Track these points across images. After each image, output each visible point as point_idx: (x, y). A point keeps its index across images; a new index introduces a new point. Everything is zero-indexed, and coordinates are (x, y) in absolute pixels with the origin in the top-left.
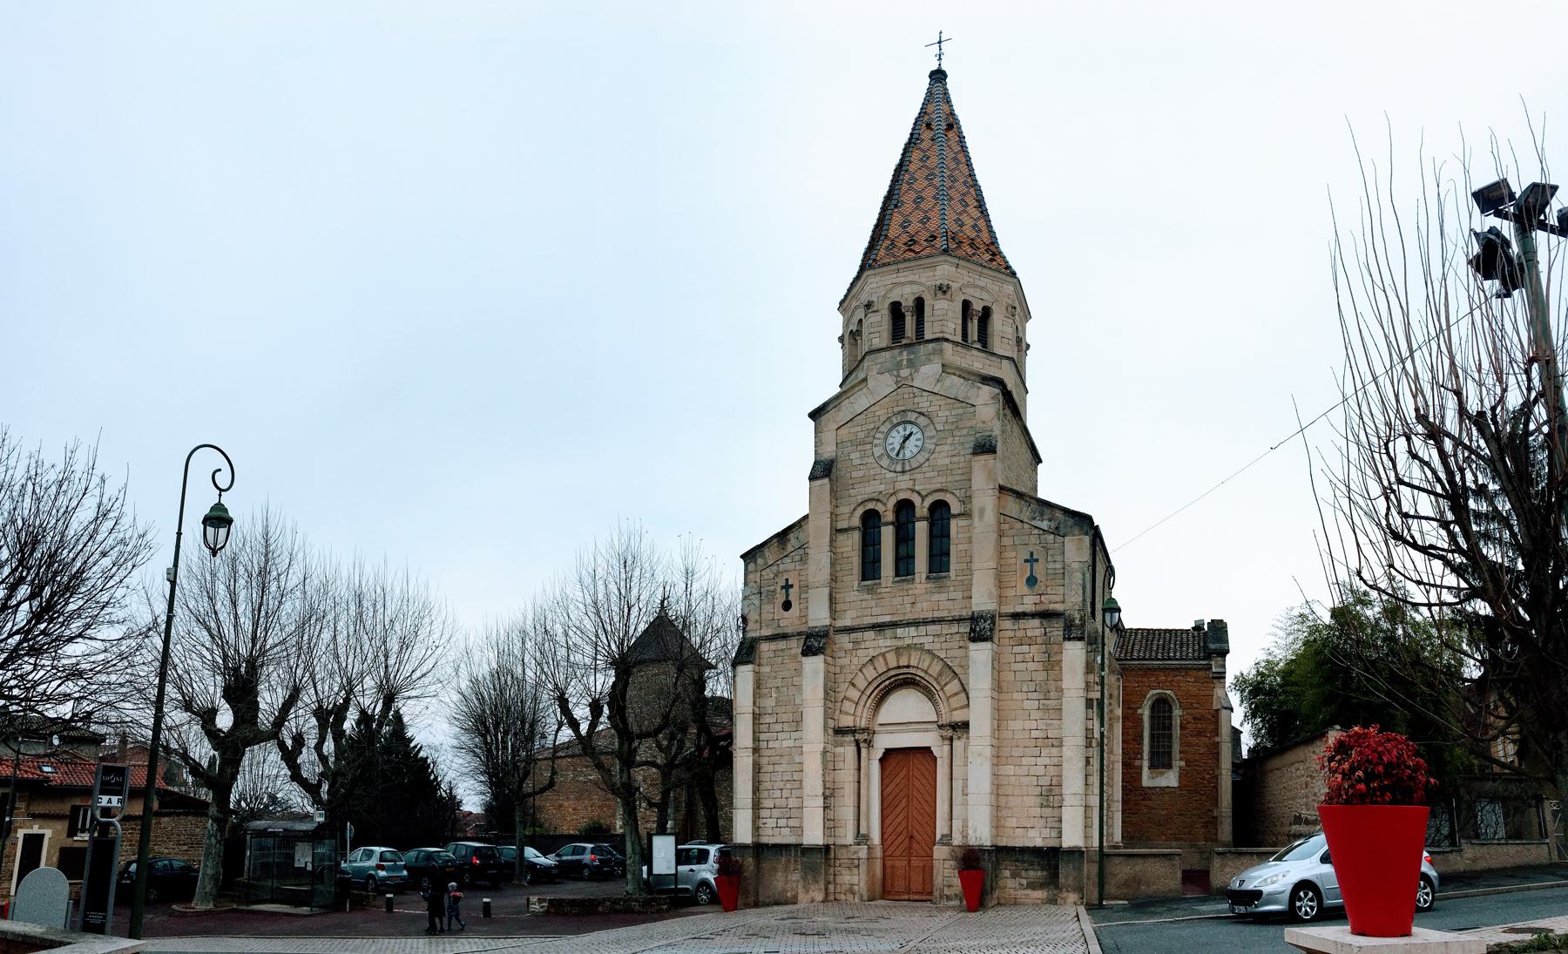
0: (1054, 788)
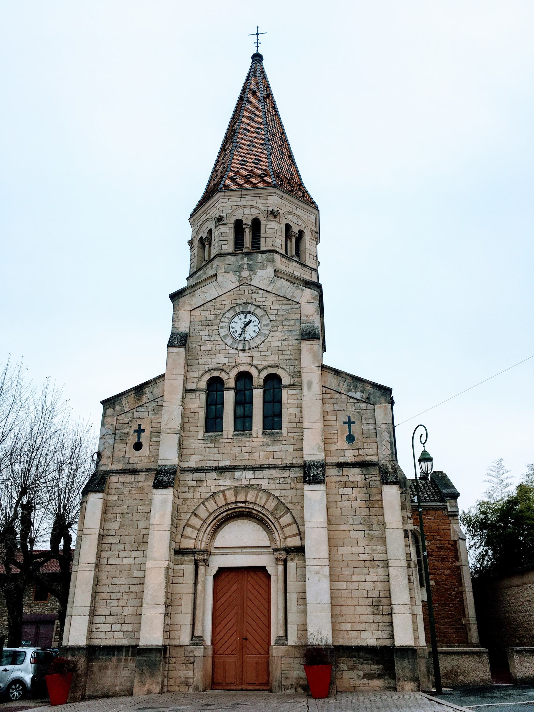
0: (382, 599)
